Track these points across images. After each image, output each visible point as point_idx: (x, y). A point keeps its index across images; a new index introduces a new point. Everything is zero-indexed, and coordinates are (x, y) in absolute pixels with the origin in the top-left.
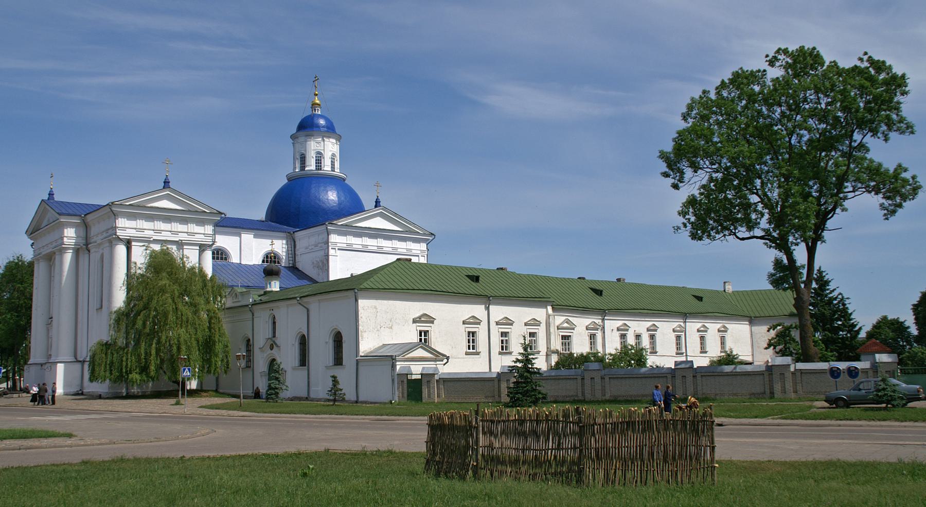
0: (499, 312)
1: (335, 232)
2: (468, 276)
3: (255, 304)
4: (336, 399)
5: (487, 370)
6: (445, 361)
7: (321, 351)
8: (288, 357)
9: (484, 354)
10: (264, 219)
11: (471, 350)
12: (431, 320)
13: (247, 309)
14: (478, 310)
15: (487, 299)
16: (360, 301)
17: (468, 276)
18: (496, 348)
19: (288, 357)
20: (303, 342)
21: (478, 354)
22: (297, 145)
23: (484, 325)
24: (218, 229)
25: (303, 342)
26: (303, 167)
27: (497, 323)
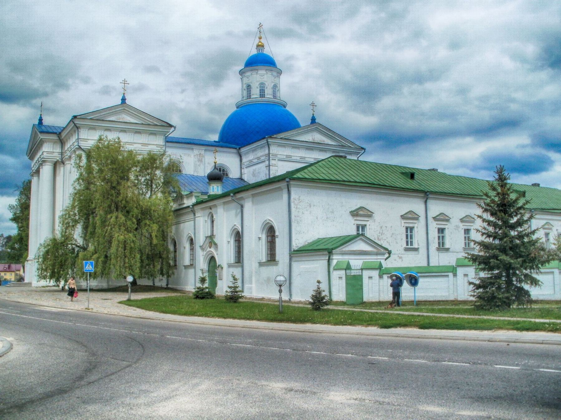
0: (437, 207)
1: (275, 144)
2: (402, 173)
3: (194, 205)
4: (234, 298)
5: (426, 265)
6: (387, 255)
7: (255, 246)
8: (225, 254)
9: (423, 250)
10: (217, 140)
11: (409, 246)
12: (369, 215)
13: (189, 210)
14: (416, 205)
15: (426, 195)
16: (365, 299)
17: (402, 173)
18: (434, 245)
19: (225, 254)
20: (238, 237)
21: (416, 250)
22: (245, 79)
23: (422, 219)
24: (168, 144)
25: (238, 237)
26: (249, 96)
27: (435, 218)
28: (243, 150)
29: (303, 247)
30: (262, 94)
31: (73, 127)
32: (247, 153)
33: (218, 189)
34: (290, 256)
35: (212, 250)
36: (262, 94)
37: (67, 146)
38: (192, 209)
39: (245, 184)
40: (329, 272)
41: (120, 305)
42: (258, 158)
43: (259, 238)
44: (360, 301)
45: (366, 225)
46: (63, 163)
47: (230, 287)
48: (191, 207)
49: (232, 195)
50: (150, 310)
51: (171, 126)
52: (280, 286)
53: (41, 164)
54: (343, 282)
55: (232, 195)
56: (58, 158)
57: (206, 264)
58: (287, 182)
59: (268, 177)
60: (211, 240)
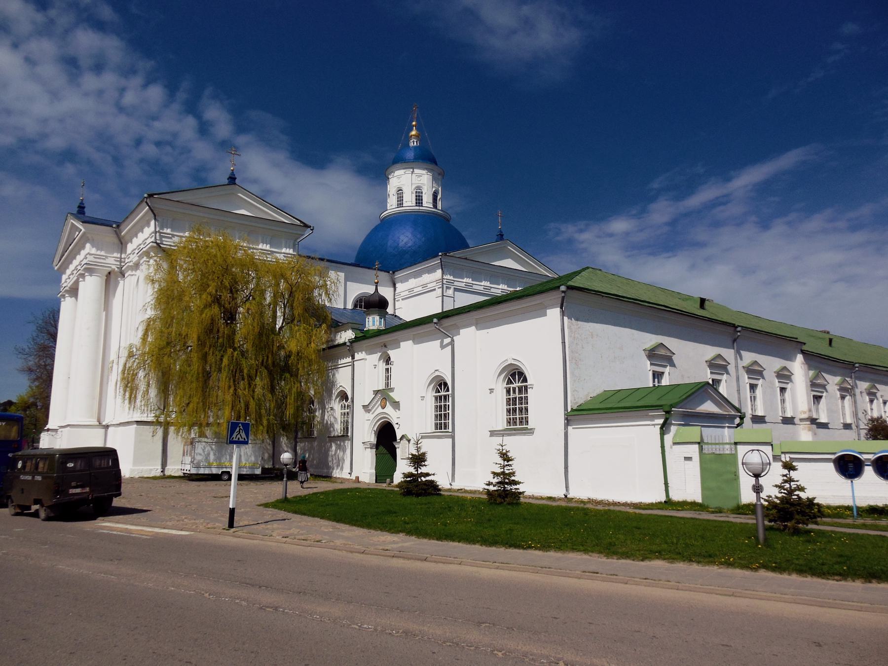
3: (352, 342)
6: (737, 421)
28: (399, 275)
29: (586, 403)
30: (419, 200)
31: (146, 213)
32: (405, 280)
33: (380, 322)
34: (566, 419)
35: (389, 409)
36: (419, 200)
37: (130, 247)
38: (350, 349)
39: (402, 322)
40: (663, 447)
41: (271, 513)
42: (424, 286)
43: (491, 390)
44: (732, 504)
45: (663, 373)
46: (123, 275)
47: (495, 474)
48: (348, 344)
49: (435, 320)
50: (392, 529)
51: (306, 226)
52: (757, 476)
53: (82, 276)
54: (694, 467)
55: (435, 320)
56: (114, 267)
57: (373, 435)
58: (563, 292)
59: (440, 311)
60: (384, 396)
